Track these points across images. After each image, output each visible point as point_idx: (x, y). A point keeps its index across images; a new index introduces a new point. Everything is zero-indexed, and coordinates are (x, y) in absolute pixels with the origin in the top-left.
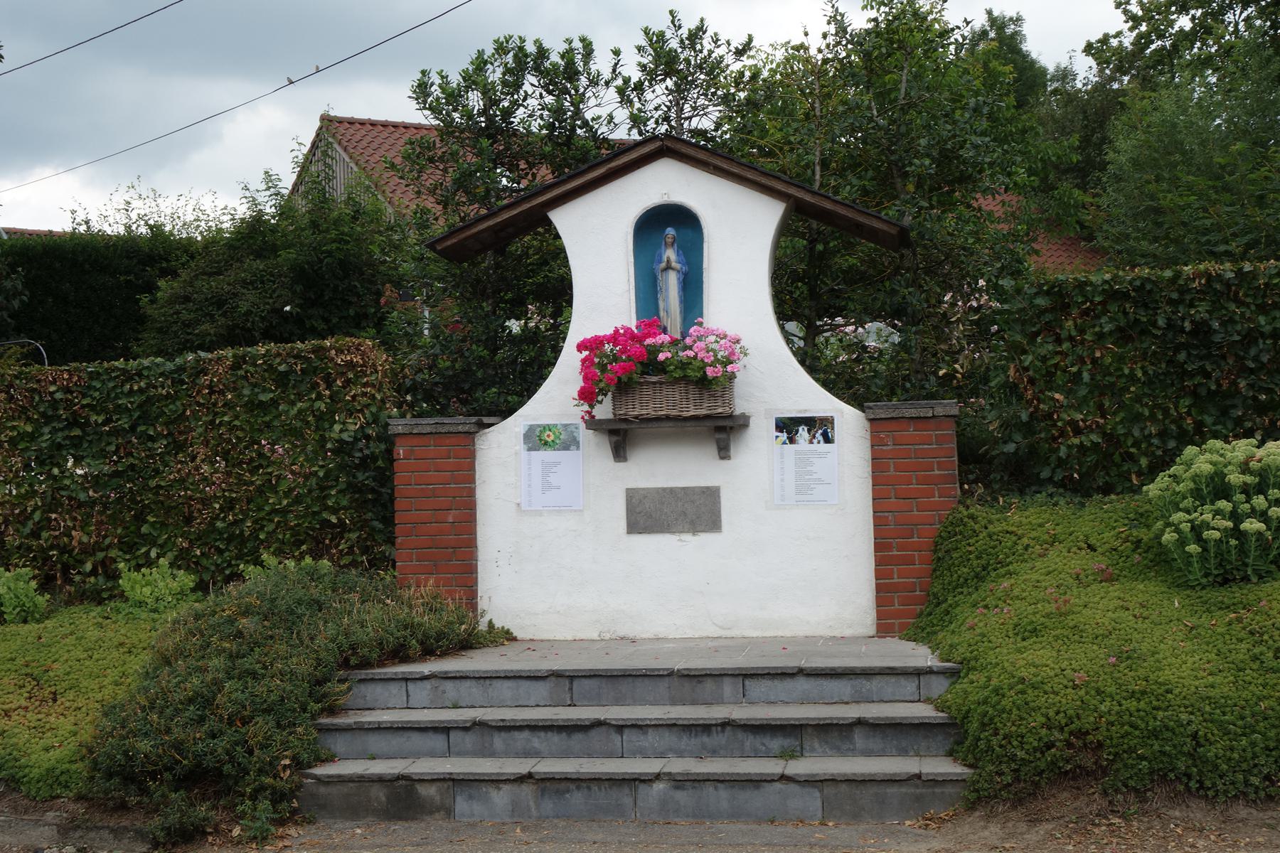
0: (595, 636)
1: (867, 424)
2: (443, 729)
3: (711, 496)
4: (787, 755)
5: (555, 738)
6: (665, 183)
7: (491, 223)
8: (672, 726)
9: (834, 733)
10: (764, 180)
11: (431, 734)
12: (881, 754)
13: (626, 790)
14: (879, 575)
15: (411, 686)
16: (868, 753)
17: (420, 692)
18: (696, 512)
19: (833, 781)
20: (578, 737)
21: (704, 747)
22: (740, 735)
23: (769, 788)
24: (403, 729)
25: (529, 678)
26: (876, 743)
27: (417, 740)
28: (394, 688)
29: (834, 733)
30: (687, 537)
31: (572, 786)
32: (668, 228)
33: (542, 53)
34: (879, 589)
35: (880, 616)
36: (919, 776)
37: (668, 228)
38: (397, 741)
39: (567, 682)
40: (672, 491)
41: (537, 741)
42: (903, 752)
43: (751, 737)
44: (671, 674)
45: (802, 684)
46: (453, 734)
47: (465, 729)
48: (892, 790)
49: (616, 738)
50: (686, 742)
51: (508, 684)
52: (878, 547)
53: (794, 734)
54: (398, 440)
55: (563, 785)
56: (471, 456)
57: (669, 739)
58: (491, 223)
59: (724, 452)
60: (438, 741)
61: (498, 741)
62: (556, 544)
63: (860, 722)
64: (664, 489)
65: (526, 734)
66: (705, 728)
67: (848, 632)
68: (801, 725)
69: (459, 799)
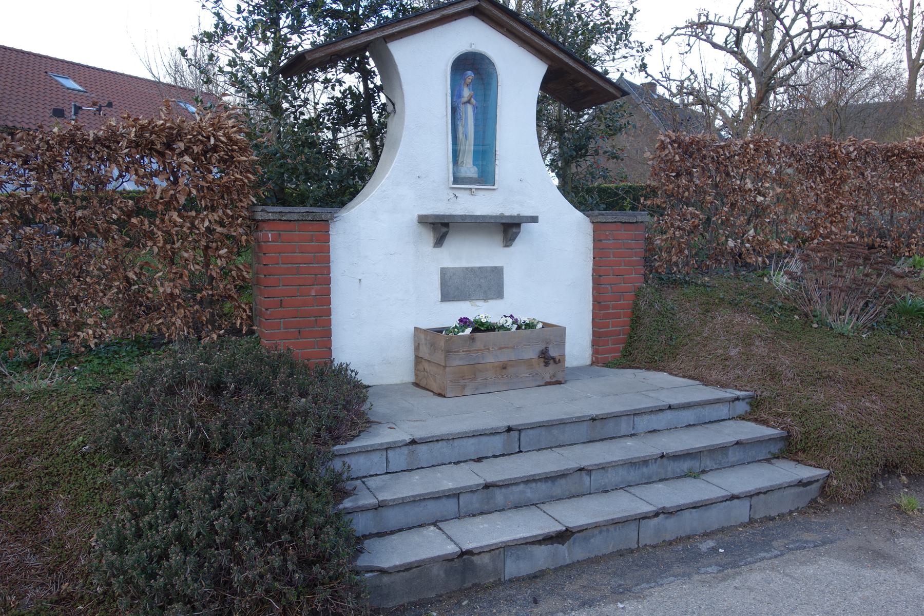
3: (497, 272)
11: (444, 500)
15: (391, 453)
31: (596, 531)
34: (595, 334)
35: (595, 352)
37: (472, 69)
39: (516, 433)
40: (472, 270)
43: (672, 463)
49: (586, 479)
50: (633, 475)
51: (472, 441)
64: (467, 268)
65: (522, 487)
69: (509, 562)
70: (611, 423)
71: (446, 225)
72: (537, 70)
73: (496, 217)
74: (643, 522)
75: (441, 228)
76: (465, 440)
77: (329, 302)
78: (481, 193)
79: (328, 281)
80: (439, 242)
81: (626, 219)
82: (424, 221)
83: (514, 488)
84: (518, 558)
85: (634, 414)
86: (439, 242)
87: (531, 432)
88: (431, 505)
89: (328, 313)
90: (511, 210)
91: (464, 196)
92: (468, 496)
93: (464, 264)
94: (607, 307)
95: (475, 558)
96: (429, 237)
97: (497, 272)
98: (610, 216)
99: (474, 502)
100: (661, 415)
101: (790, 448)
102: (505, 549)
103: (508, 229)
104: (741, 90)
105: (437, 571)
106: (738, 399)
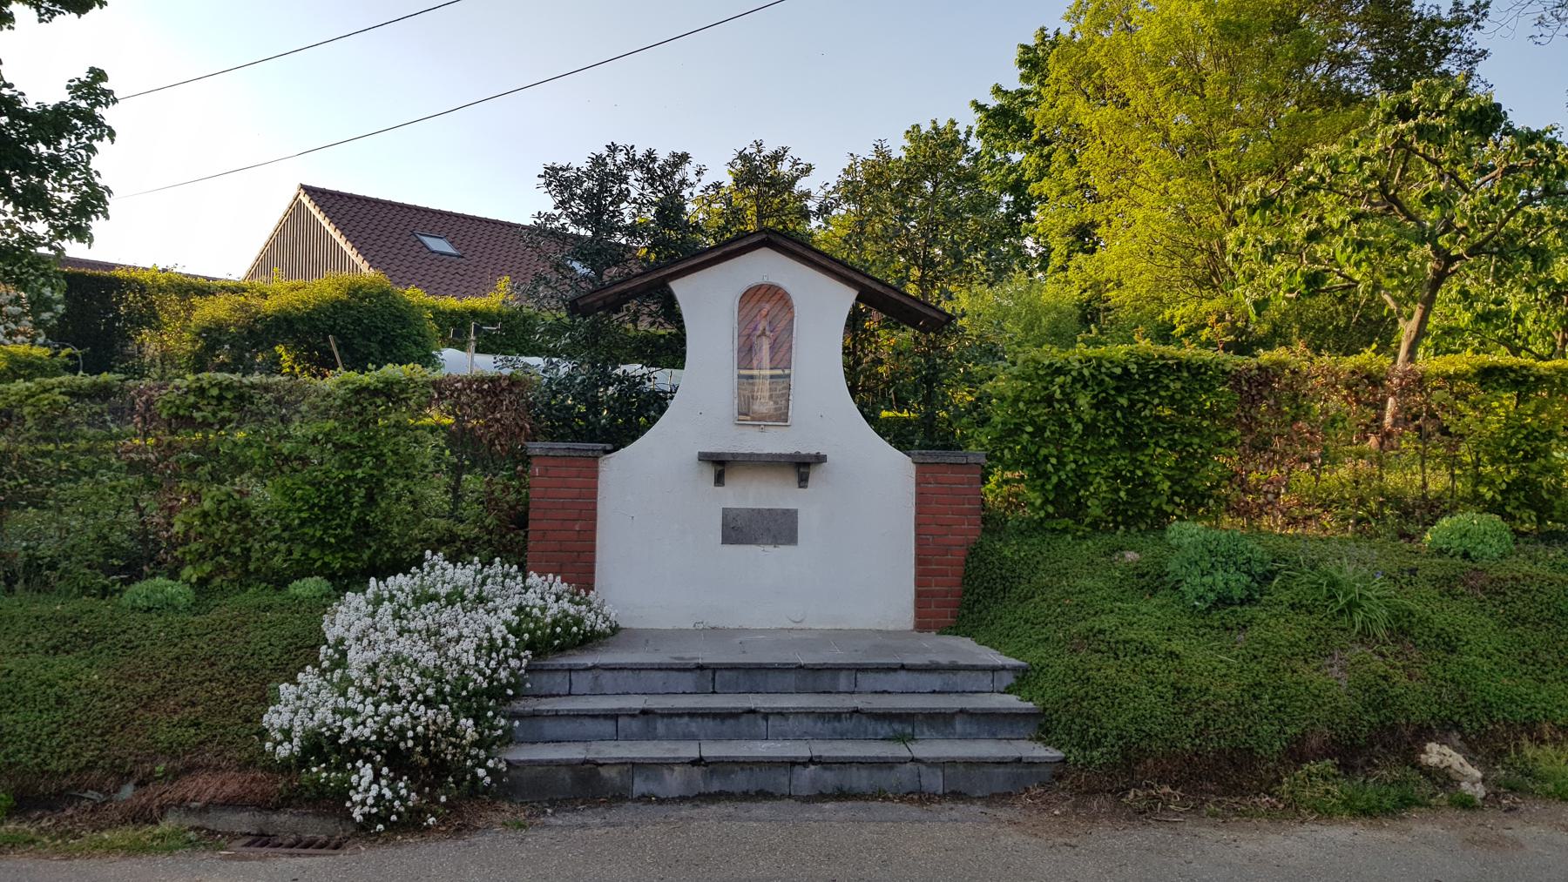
1: (913, 467)
2: (613, 716)
3: (790, 517)
6: (766, 267)
7: (625, 287)
8: (809, 713)
9: (940, 721)
11: (601, 720)
12: (976, 738)
14: (918, 583)
15: (574, 675)
16: (964, 737)
17: (582, 682)
18: (778, 529)
19: (953, 762)
21: (834, 731)
25: (679, 670)
26: (972, 729)
27: (590, 726)
28: (559, 678)
29: (940, 721)
30: (770, 548)
32: (766, 301)
33: (651, 156)
34: (919, 594)
35: (918, 615)
36: (1019, 760)
37: (766, 301)
38: (569, 727)
39: (709, 674)
41: (694, 726)
42: (994, 736)
44: (801, 667)
45: (902, 676)
46: (771, 718)
51: (661, 674)
53: (904, 723)
54: (534, 460)
55: (729, 767)
56: (595, 476)
57: (808, 723)
58: (625, 287)
60: (608, 727)
61: (661, 726)
62: (660, 548)
63: (962, 711)
65: (686, 719)
66: (837, 715)
67: (891, 628)
68: (908, 715)
69: (637, 780)
70: (827, 676)
72: (846, 297)
74: (798, 769)
75: (721, 466)
76: (653, 674)
80: (719, 480)
81: (952, 460)
82: (705, 458)
84: (647, 777)
86: (719, 480)
87: (727, 674)
89: (592, 549)
90: (808, 448)
91: (751, 433)
92: (627, 720)
95: (603, 771)
96: (709, 473)
97: (790, 517)
98: (932, 456)
99: (635, 725)
100: (892, 676)
101: (1041, 725)
102: (635, 766)
103: (802, 467)
104: (1453, 272)
106: (1003, 668)
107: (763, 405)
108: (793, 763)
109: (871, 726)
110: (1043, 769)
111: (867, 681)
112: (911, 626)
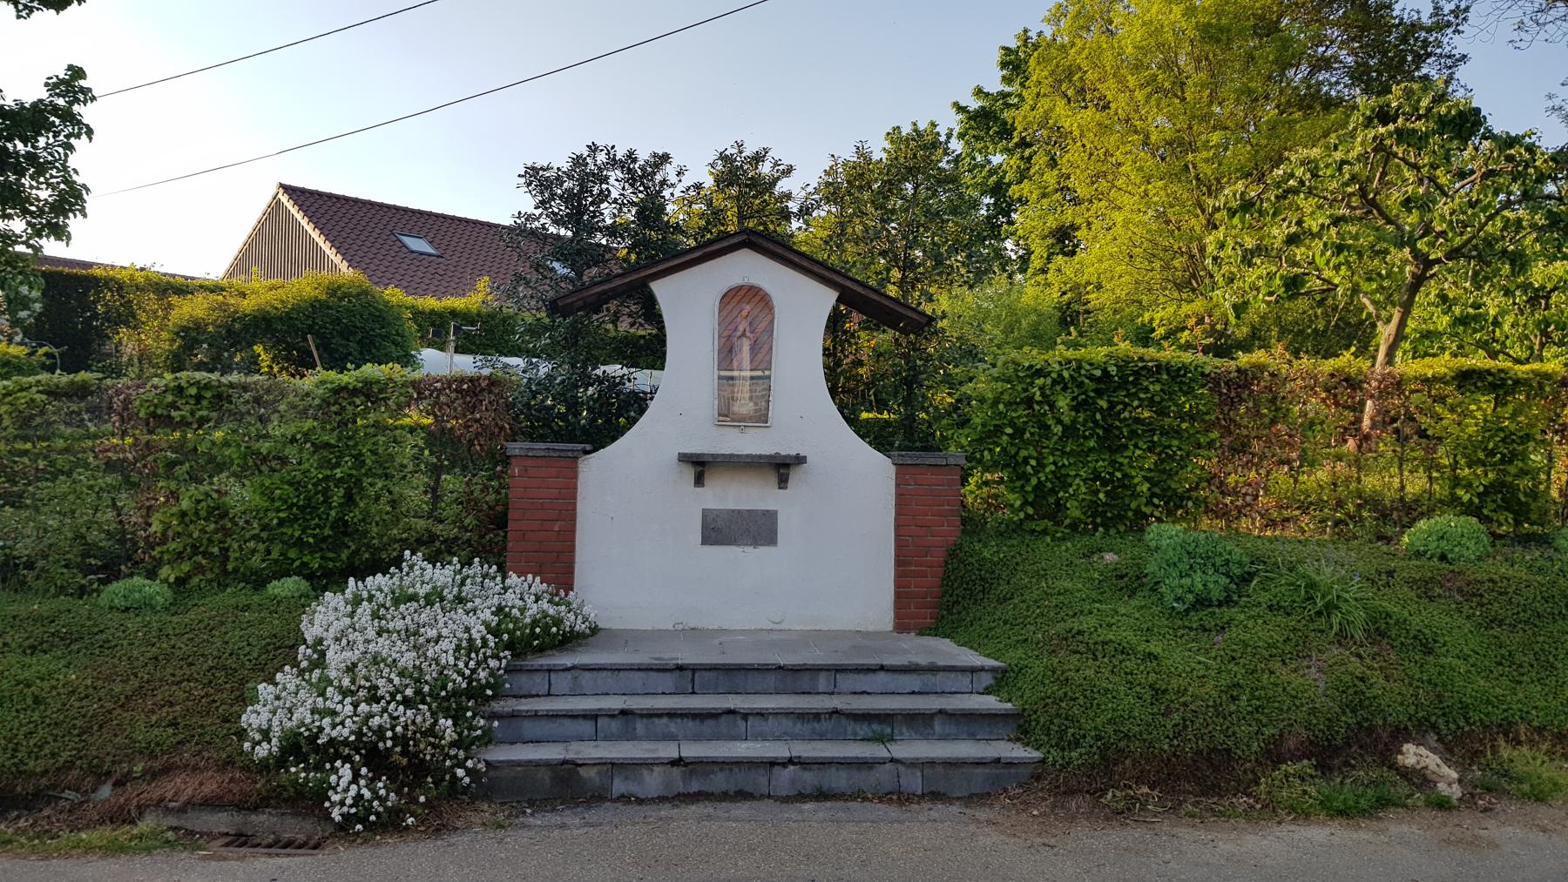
0: (670, 627)
1: (893, 468)
2: (593, 716)
3: (770, 517)
4: (880, 739)
5: (690, 724)
7: (606, 287)
9: (919, 722)
10: (827, 274)
11: (581, 721)
13: (762, 771)
14: (897, 585)
15: (553, 676)
16: (944, 738)
17: (561, 682)
18: (757, 530)
19: (932, 763)
20: (711, 722)
22: (844, 721)
23: (723, 719)
24: (557, 716)
25: (658, 670)
26: (951, 729)
27: (570, 727)
30: (749, 549)
31: (716, 768)
33: (631, 157)
34: (898, 595)
35: (897, 616)
36: (998, 760)
37: (746, 301)
39: (689, 674)
41: (674, 727)
42: (972, 737)
46: (751, 719)
47: (612, 716)
48: (979, 770)
49: (741, 724)
51: (641, 674)
52: (900, 562)
53: (883, 724)
54: (513, 460)
58: (606, 287)
59: (783, 482)
60: (586, 727)
61: (640, 726)
62: (641, 549)
65: (665, 720)
66: (817, 716)
67: (871, 628)
69: (617, 782)
71: (787, 466)
73: (771, 456)
75: (701, 467)
77: (573, 540)
78: (752, 431)
79: (573, 518)
82: (685, 459)
83: (656, 720)
84: (627, 778)
85: (837, 671)
86: (699, 481)
88: (567, 722)
92: (607, 720)
93: (731, 505)
94: (909, 563)
96: (689, 473)
97: (770, 517)
98: (911, 458)
99: (615, 725)
100: (870, 677)
101: (1020, 726)
102: (615, 766)
103: (782, 468)
105: (545, 776)
106: (982, 669)
107: (744, 406)
108: (773, 763)
109: (851, 726)
110: (1021, 770)
111: (846, 682)
112: (890, 627)
